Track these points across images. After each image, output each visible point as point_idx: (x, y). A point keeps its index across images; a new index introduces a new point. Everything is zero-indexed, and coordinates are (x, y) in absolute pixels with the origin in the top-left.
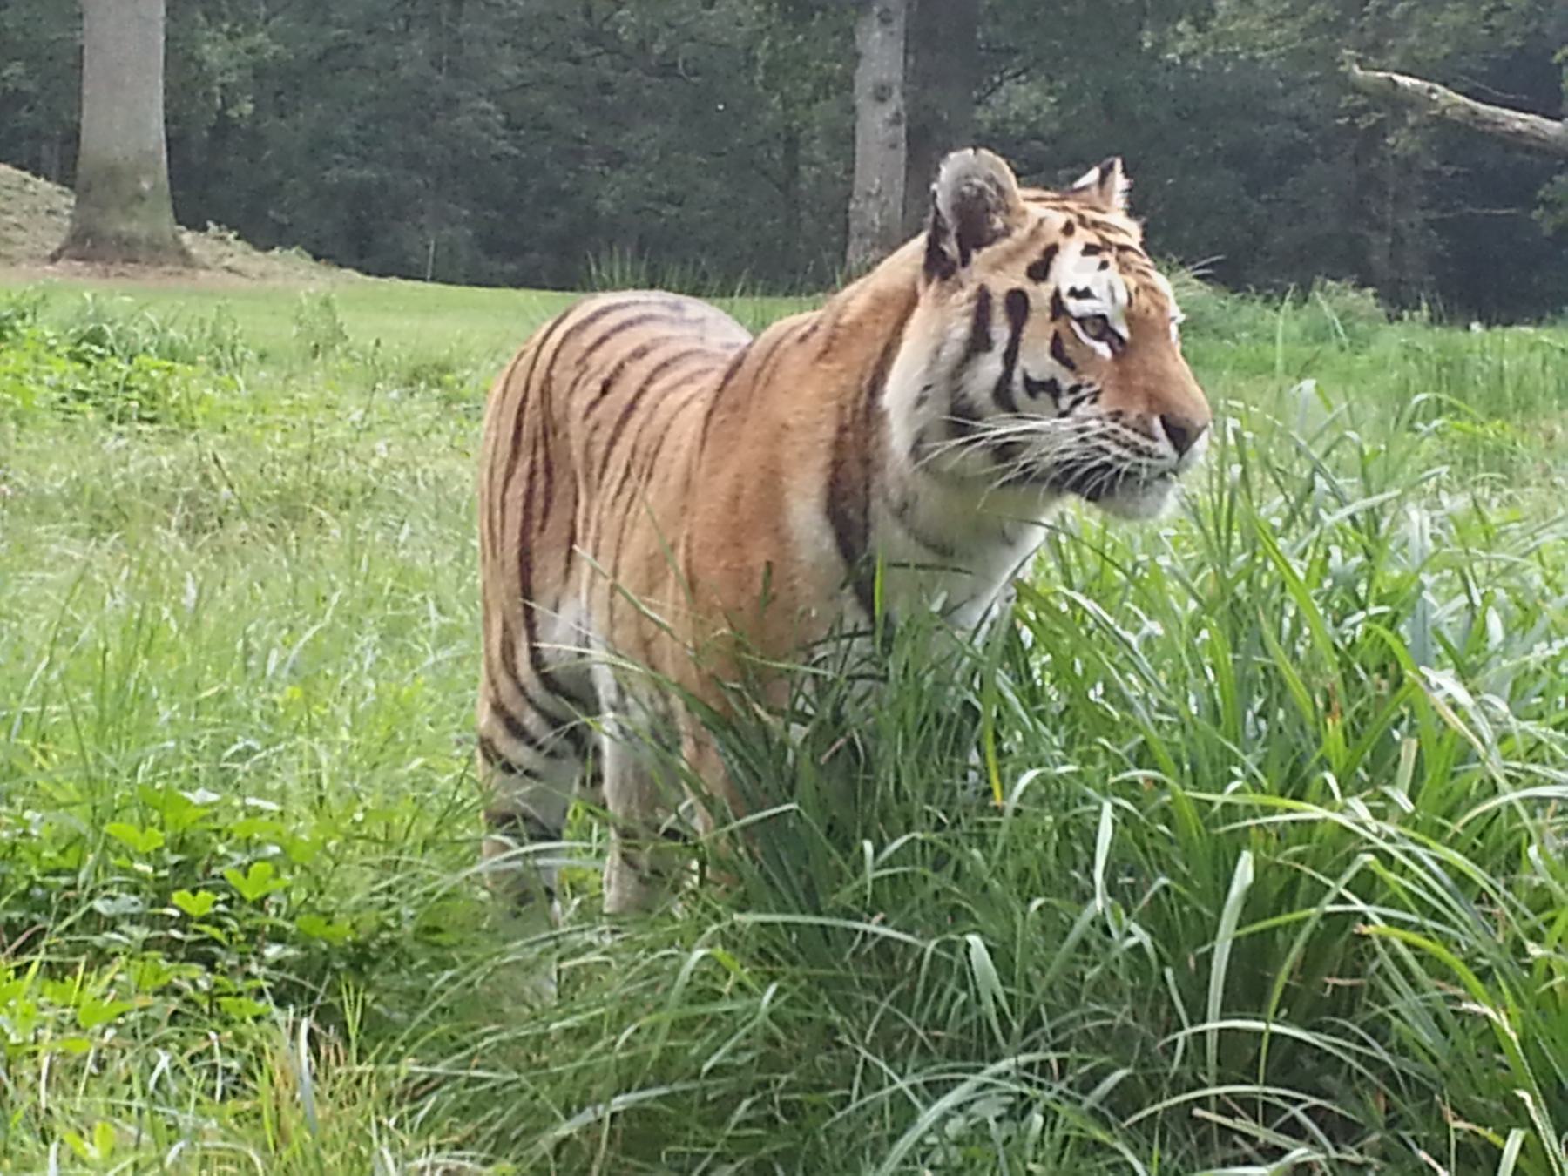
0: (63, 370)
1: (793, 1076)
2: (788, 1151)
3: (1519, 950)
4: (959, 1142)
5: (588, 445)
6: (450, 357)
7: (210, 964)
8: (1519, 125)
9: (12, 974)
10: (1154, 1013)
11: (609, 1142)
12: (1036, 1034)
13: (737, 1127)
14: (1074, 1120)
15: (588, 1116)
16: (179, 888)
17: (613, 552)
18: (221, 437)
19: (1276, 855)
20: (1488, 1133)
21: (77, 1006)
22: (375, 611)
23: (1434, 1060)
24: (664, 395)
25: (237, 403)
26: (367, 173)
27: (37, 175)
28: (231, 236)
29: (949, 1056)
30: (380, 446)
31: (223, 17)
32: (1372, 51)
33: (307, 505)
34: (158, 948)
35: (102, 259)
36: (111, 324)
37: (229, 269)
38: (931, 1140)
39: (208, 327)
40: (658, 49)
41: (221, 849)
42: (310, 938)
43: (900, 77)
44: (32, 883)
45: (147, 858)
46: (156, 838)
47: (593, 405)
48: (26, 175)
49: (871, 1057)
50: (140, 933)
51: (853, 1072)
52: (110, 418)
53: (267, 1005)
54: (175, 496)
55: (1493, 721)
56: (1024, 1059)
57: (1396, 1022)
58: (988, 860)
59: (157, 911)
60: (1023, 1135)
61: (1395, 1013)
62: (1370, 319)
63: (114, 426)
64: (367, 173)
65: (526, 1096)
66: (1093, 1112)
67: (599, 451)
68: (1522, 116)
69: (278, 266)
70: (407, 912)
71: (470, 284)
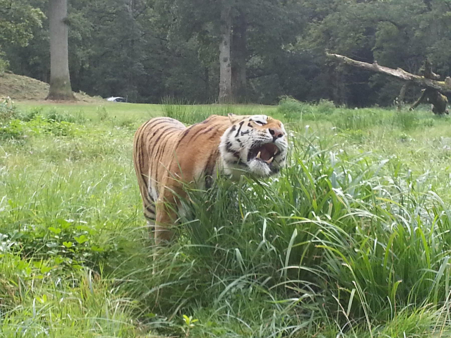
0: (46, 125)
1: (199, 279)
2: (198, 296)
3: (353, 248)
4: (234, 293)
5: (150, 146)
6: (131, 120)
7: (71, 257)
8: (363, 65)
9: (26, 262)
10: (277, 264)
11: (159, 295)
12: (251, 269)
13: (187, 291)
14: (260, 289)
15: (153, 289)
16: (65, 241)
17: (156, 168)
18: (80, 139)
19: (302, 229)
20: (347, 290)
21: (41, 268)
22: (112, 177)
23: (337, 273)
24: (166, 135)
25: (84, 131)
26: (114, 79)
27: (42, 81)
28: (85, 93)
29: (233, 275)
30: (115, 140)
31: (81, 46)
32: (332, 49)
33: (98, 154)
34: (61, 254)
35: (56, 99)
36: (57, 114)
37: (84, 101)
38: (228, 293)
39: (78, 114)
40: (177, 51)
41: (74, 232)
42: (94, 251)
43: (229, 57)
44: (33, 241)
45: (58, 234)
46: (59, 231)
47: (151, 138)
48: (39, 81)
49: (216, 276)
50: (57, 251)
51: (212, 278)
52: (56, 135)
53: (83, 266)
54: (70, 152)
55: (348, 199)
56: (248, 275)
57: (329, 266)
58: (240, 231)
59: (60, 246)
60: (248, 292)
61: (328, 264)
62: (333, 107)
63: (57, 137)
64: (114, 79)
65: (141, 285)
66: (264, 287)
67: (151, 147)
68: (364, 63)
69: (95, 100)
70: (115, 245)
71: (137, 103)
